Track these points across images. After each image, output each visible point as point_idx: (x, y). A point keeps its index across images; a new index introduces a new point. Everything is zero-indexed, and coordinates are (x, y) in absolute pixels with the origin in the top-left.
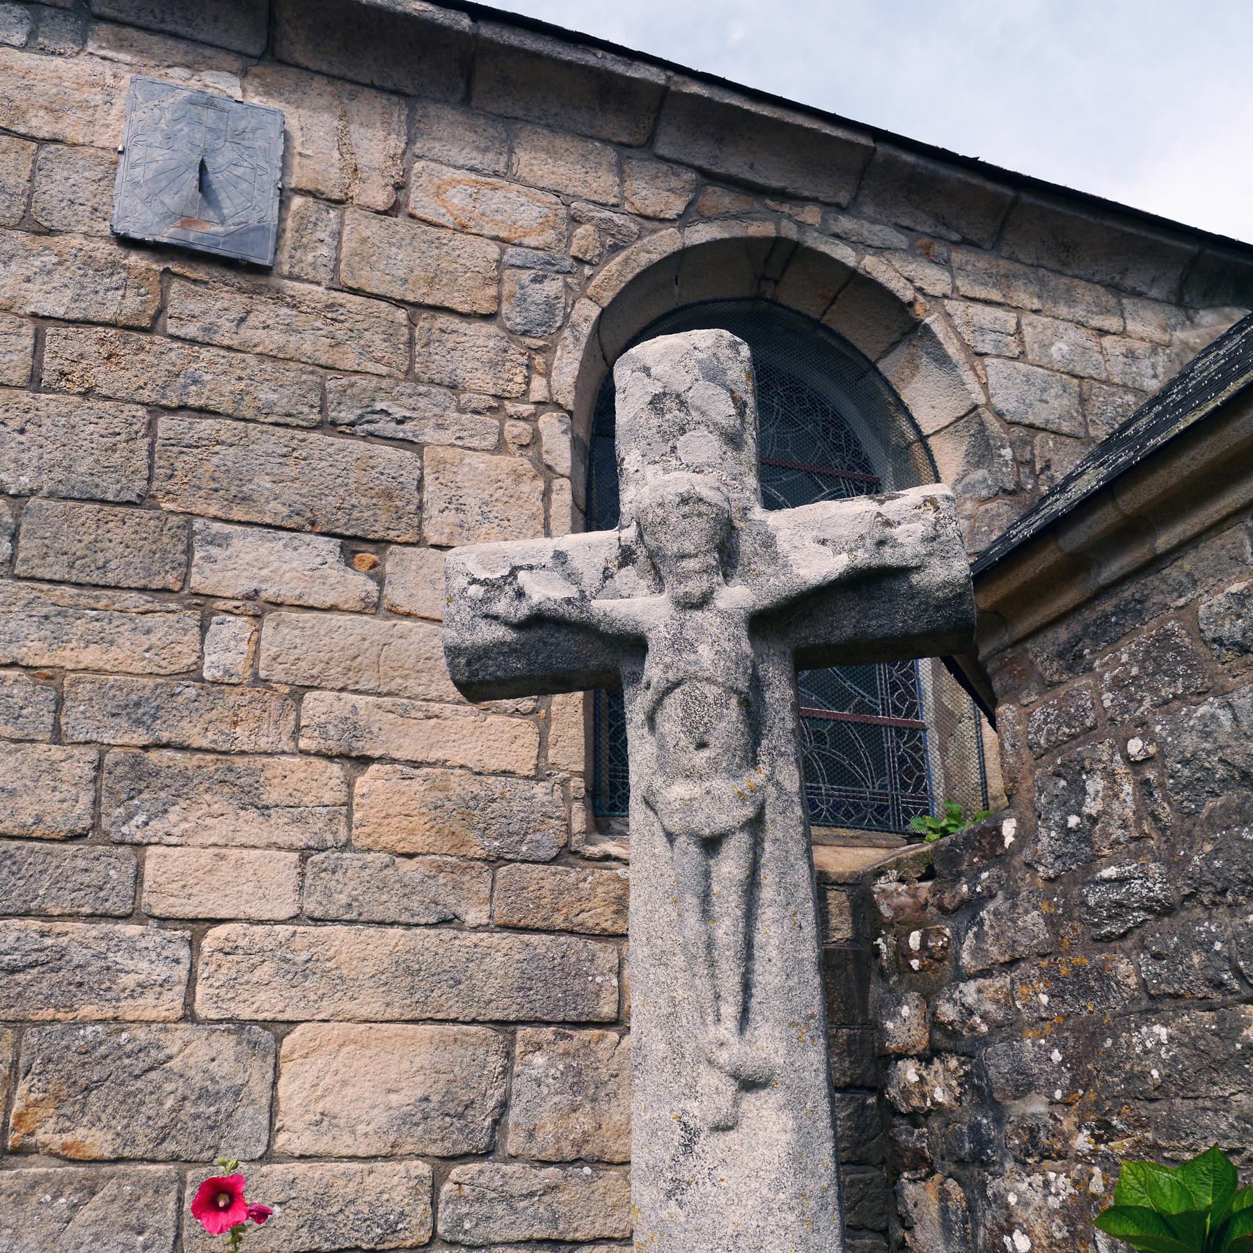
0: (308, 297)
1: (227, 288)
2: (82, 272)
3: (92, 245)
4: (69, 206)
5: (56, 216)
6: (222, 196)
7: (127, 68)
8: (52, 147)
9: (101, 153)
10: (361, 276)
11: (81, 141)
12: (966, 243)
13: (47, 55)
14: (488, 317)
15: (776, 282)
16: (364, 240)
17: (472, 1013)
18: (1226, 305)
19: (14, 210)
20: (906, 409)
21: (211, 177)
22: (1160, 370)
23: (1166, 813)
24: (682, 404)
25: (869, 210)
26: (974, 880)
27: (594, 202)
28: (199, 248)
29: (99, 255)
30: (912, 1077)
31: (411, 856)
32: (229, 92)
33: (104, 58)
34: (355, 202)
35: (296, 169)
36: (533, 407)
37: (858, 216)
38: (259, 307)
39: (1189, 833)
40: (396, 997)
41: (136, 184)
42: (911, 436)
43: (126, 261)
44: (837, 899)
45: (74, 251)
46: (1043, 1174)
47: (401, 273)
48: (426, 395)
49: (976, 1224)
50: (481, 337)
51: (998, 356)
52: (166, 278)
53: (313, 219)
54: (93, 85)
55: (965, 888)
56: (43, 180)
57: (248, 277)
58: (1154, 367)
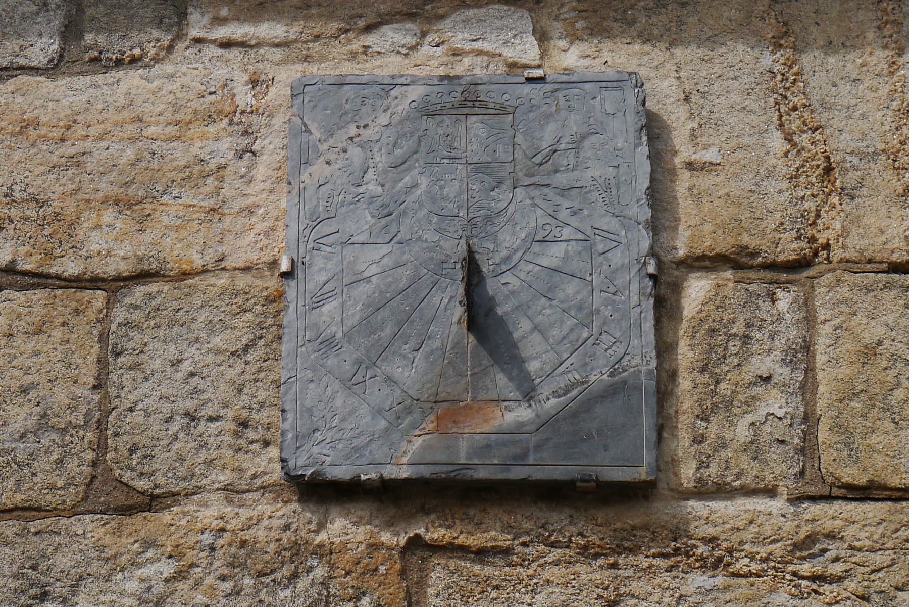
0: (748, 536)
1: (556, 554)
2: (228, 586)
3: (245, 513)
4: (186, 429)
5: (161, 461)
6: (521, 328)
7: (278, 54)
8: (139, 292)
9: (243, 281)
10: (872, 449)
11: (198, 262)
13: (107, 69)
16: (869, 353)
19: (72, 465)
21: (492, 286)
28: (482, 474)
29: (260, 533)
32: (510, 54)
33: (227, 45)
34: (837, 254)
35: (685, 207)
38: (635, 587)
41: (329, 344)
43: (322, 537)
45: (207, 538)
52: (415, 560)
53: (738, 328)
54: (210, 119)
56: (127, 377)
57: (601, 516)
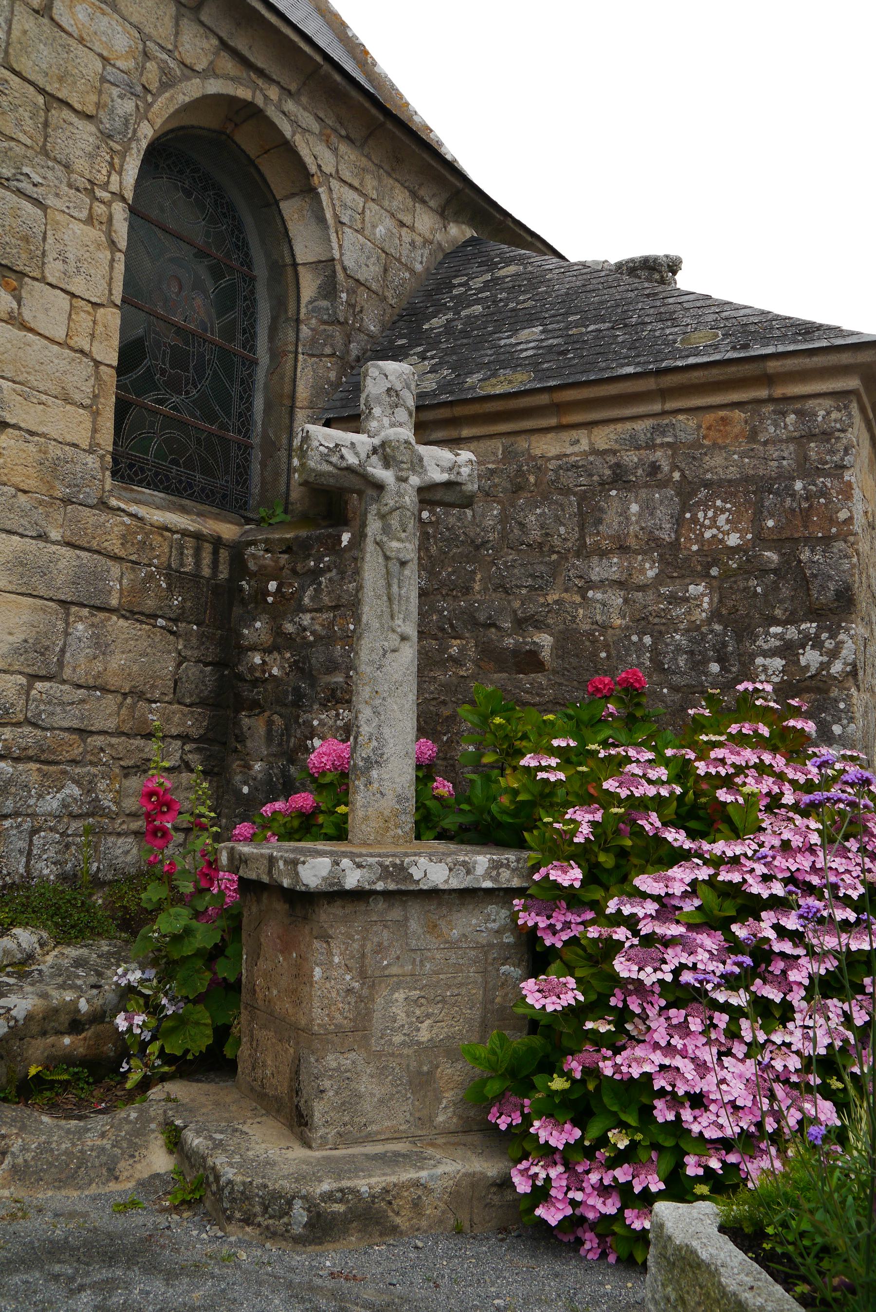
12: (348, 139)
14: (89, 117)
15: (236, 125)
17: (51, 594)
18: (463, 223)
20: (290, 241)
22: (425, 259)
23: (433, 550)
24: (397, 395)
25: (304, 100)
26: (319, 560)
27: (159, 44)
30: (258, 660)
31: (25, 492)
36: (109, 195)
37: (298, 102)
39: (442, 561)
40: (14, 578)
42: (288, 260)
44: (224, 554)
46: (337, 710)
47: (44, 66)
48: (53, 169)
49: (289, 736)
50: (85, 132)
51: (350, 227)
55: (312, 563)
58: (422, 256)
